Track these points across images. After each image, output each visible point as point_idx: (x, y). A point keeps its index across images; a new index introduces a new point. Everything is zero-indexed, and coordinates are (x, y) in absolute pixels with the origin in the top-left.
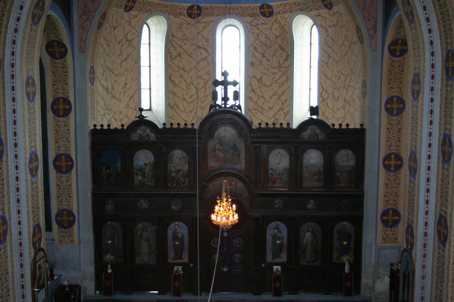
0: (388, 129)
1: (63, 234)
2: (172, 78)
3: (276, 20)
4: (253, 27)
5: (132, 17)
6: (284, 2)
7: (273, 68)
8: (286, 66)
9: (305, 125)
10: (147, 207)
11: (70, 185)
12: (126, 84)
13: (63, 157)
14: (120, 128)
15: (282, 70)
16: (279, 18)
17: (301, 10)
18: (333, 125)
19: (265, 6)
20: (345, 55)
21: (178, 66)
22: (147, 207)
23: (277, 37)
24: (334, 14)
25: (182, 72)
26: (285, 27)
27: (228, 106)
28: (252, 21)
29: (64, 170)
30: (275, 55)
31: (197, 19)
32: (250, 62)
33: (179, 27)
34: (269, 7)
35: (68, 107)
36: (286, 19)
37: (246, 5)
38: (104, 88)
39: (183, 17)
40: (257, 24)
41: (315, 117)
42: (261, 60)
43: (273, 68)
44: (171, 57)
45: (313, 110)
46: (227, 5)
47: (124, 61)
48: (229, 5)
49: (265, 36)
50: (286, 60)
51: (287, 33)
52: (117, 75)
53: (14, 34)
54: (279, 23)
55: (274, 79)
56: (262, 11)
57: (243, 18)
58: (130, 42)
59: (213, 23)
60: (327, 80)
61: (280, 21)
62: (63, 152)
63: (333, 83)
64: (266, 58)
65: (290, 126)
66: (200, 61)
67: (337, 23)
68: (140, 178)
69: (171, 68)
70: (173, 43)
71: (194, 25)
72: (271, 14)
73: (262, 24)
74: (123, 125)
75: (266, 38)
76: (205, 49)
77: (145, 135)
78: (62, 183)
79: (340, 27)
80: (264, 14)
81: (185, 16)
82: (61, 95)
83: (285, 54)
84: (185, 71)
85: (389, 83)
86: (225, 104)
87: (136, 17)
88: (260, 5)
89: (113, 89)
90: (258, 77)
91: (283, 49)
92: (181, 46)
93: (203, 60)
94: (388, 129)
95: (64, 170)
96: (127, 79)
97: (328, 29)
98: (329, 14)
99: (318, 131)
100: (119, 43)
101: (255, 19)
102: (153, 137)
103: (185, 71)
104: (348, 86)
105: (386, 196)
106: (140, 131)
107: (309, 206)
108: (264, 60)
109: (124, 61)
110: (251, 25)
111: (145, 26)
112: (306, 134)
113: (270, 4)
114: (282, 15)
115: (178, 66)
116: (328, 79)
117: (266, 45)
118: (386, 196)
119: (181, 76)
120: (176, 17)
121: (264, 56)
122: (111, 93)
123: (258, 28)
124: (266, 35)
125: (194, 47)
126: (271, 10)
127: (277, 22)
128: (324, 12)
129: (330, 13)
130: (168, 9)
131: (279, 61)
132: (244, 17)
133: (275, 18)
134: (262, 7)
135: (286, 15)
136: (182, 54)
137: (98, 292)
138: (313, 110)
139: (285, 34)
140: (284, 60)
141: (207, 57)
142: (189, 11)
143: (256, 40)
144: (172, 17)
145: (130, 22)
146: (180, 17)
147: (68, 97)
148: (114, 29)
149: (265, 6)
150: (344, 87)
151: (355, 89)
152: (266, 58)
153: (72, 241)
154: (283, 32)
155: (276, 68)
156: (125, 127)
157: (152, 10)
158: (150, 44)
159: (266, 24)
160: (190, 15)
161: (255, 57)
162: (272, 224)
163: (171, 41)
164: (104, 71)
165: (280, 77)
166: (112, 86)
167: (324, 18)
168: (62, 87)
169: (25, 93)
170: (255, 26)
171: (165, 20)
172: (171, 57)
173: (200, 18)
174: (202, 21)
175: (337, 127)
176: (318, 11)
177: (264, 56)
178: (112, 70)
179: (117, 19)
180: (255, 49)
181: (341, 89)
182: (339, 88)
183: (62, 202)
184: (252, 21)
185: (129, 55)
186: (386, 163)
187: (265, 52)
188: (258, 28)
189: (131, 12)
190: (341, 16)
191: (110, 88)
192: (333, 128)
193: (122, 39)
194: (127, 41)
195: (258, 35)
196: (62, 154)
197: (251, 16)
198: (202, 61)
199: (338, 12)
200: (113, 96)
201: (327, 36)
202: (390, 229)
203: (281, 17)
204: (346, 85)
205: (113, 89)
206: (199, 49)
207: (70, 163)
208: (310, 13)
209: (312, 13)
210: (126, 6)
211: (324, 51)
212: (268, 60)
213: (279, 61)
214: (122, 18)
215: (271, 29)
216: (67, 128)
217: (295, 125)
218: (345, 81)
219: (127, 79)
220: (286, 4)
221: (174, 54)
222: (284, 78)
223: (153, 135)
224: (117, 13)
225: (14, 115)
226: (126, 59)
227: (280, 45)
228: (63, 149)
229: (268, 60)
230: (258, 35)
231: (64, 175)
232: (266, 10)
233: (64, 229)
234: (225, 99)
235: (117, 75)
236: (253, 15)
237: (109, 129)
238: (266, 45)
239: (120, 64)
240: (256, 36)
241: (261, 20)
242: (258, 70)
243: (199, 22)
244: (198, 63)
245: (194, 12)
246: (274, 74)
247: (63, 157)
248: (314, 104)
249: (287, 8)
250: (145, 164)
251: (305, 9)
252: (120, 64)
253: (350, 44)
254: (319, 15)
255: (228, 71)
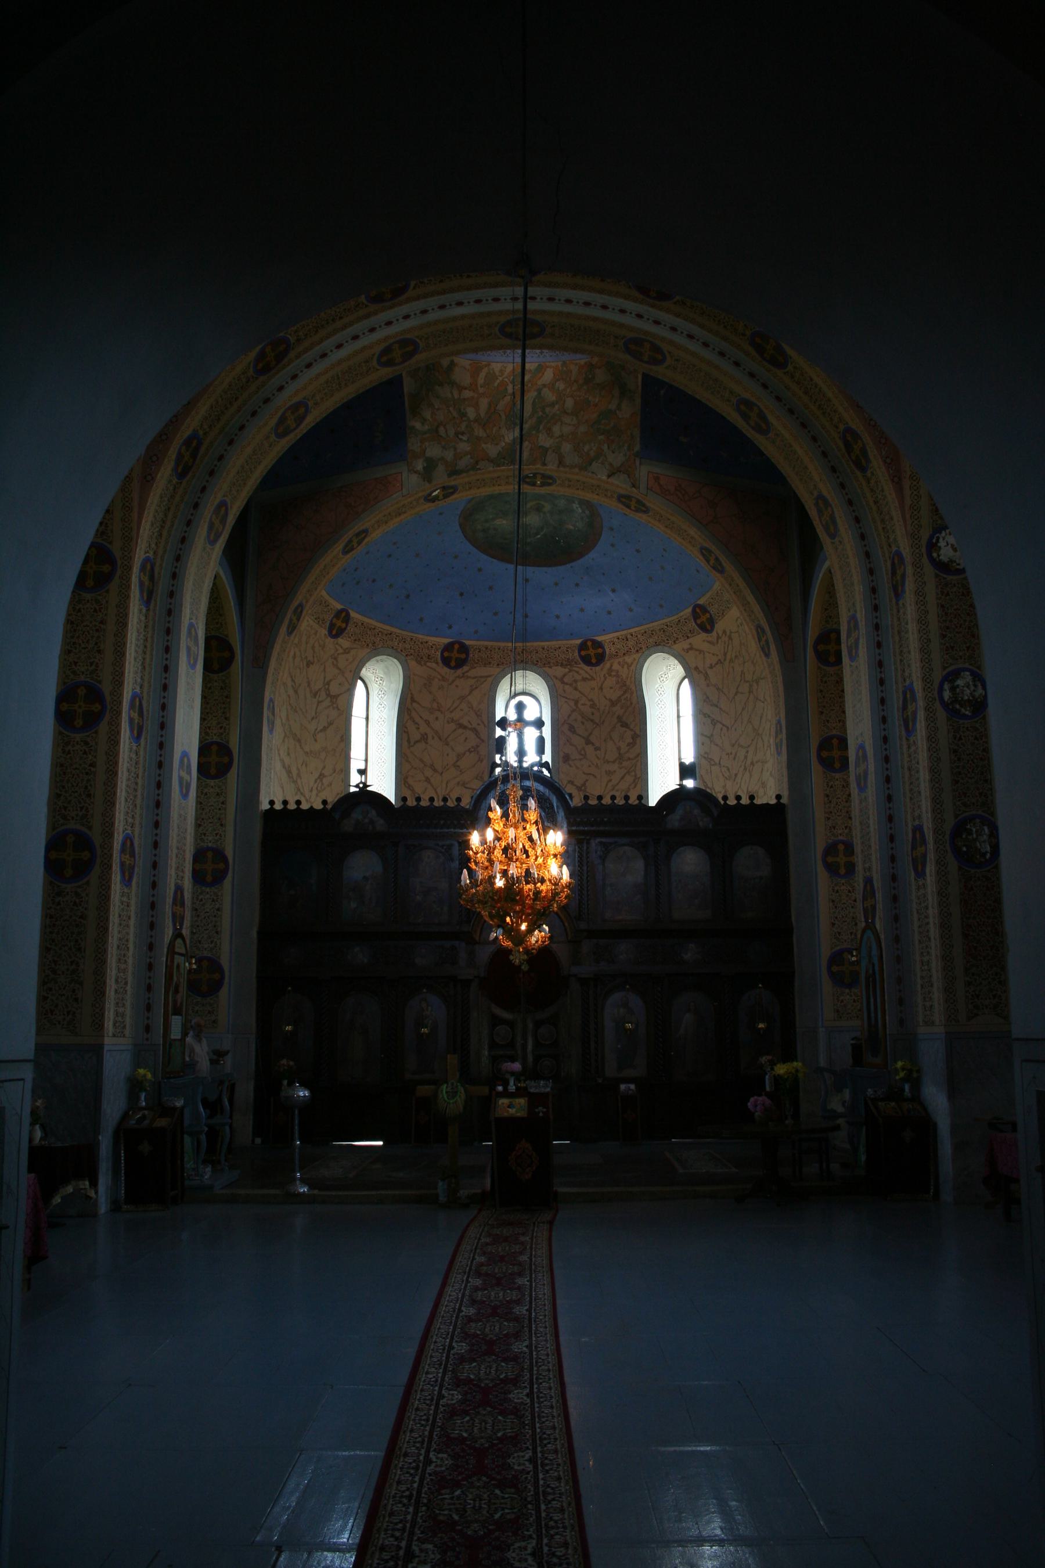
0: (828, 796)
1: (197, 1008)
2: (410, 781)
3: (610, 670)
4: (567, 687)
5: (341, 651)
6: (625, 632)
7: (608, 762)
8: (631, 756)
9: (670, 799)
10: (366, 961)
11: (218, 910)
12: (322, 776)
13: (210, 854)
14: (321, 807)
15: (625, 764)
16: (616, 667)
17: (657, 644)
18: (725, 798)
19: (589, 644)
20: (743, 709)
21: (421, 760)
22: (366, 961)
23: (613, 704)
24: (718, 638)
25: (429, 773)
26: (628, 683)
27: (525, 765)
28: (564, 676)
29: (209, 878)
30: (611, 738)
31: (459, 672)
32: (562, 754)
33: (425, 684)
34: (598, 645)
35: (226, 760)
36: (629, 666)
37: (554, 643)
38: (284, 767)
39: (434, 665)
40: (576, 681)
41: (690, 783)
42: (583, 749)
43: (608, 762)
44: (409, 741)
45: (685, 771)
46: (518, 644)
47: (321, 731)
48: (520, 644)
49: (589, 703)
50: (631, 745)
51: (632, 693)
52: (306, 753)
53: (180, 546)
54: (617, 676)
55: (610, 784)
56: (583, 653)
57: (546, 669)
58: (334, 698)
59: (490, 679)
60: (713, 768)
61: (618, 672)
62: (210, 845)
63: (724, 769)
64: (593, 744)
65: (643, 802)
66: (464, 754)
67: (725, 654)
68: (353, 905)
69: (407, 761)
70: (414, 714)
71: (453, 681)
72: (601, 658)
73: (584, 679)
74: (325, 802)
75: (592, 706)
76: (475, 731)
77: (366, 821)
78: (203, 905)
79: (731, 661)
80: (587, 661)
81: (437, 663)
82: (215, 739)
83: (629, 733)
84: (435, 770)
85: (822, 713)
86: (520, 761)
87: (346, 651)
88: (579, 642)
89: (299, 775)
90: (579, 783)
91: (625, 725)
92: (427, 722)
93: (469, 751)
94: (828, 796)
95: (209, 878)
96: (324, 767)
97: (709, 672)
98: (708, 642)
99: (696, 812)
100: (315, 695)
101: (570, 671)
102: (380, 824)
103: (435, 770)
104: (752, 763)
105: (833, 924)
106: (357, 815)
107: (688, 956)
108: (590, 749)
109: (321, 731)
110: (563, 682)
111: (360, 683)
112: (674, 820)
113: (599, 639)
114: (621, 660)
115: (421, 760)
116: (715, 764)
117: (592, 721)
118: (833, 924)
119: (428, 780)
120: (419, 663)
121: (588, 742)
122: (295, 782)
123: (576, 689)
124: (591, 700)
125: (453, 726)
126: (600, 651)
127: (613, 673)
128: (700, 639)
129: (710, 639)
130: (407, 646)
131: (619, 749)
132: (550, 667)
133: (608, 665)
134: (583, 647)
135: (628, 659)
136: (430, 738)
137: (258, 1141)
138: (685, 771)
139: (628, 695)
140: (628, 745)
141: (478, 746)
142: (446, 654)
143: (574, 711)
144: (413, 663)
145: (336, 659)
146: (429, 664)
147: (228, 742)
148: (308, 666)
149: (589, 644)
150: (745, 769)
151: (764, 762)
152: (593, 744)
153: (214, 1022)
154: (625, 692)
155: (614, 762)
156: (329, 807)
157: (376, 646)
158: (367, 718)
159: (593, 679)
160: (446, 661)
161: (571, 744)
162: (616, 997)
163: (408, 709)
164: (286, 736)
165: (623, 778)
166: (298, 769)
167: (700, 651)
168: (219, 723)
169: (279, 414)
170: (571, 685)
171: (400, 667)
172: (409, 741)
173: (465, 668)
174: (469, 674)
175: (732, 802)
176: (688, 641)
177: (588, 742)
178: (299, 741)
179: (313, 647)
180: (572, 729)
181: (740, 776)
182: (736, 775)
183: (200, 942)
184: (564, 676)
185: (330, 724)
186: (830, 859)
187: (591, 734)
188: (576, 689)
189: (340, 640)
190: (730, 638)
191: (295, 772)
192: (725, 803)
193: (320, 690)
194: (328, 695)
195: (576, 702)
196: (208, 849)
197: (562, 665)
198: (468, 753)
199: (724, 632)
200: (299, 790)
201: (708, 686)
202: (847, 991)
203: (619, 663)
204: (749, 762)
205: (299, 775)
206: (460, 731)
207: (221, 866)
208: (675, 647)
209: (678, 647)
210: (332, 626)
211: (705, 715)
212: (597, 749)
213: (619, 749)
214: (323, 647)
215: (601, 689)
216: (222, 799)
217: (653, 801)
218: (746, 757)
219: (324, 767)
220: (629, 636)
221: (416, 736)
222: (629, 779)
223: (382, 821)
224: (316, 634)
225: (164, 675)
226: (325, 729)
227: (619, 718)
228: (210, 838)
229: (597, 749)
230: (576, 702)
231: (208, 890)
232: (592, 652)
233: (199, 999)
234: (521, 753)
235: (306, 753)
236: (568, 663)
237: (298, 809)
238: (592, 721)
239: (314, 735)
240: (572, 704)
241: (581, 672)
242: (577, 768)
243: (463, 676)
244: (459, 757)
245: (456, 656)
246: (609, 773)
247: (210, 854)
248: (689, 758)
249: (631, 643)
250: (365, 878)
251: (663, 641)
252: (314, 735)
253: (751, 686)
254: (691, 648)
255: (525, 702)
